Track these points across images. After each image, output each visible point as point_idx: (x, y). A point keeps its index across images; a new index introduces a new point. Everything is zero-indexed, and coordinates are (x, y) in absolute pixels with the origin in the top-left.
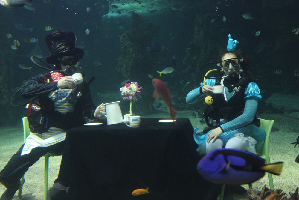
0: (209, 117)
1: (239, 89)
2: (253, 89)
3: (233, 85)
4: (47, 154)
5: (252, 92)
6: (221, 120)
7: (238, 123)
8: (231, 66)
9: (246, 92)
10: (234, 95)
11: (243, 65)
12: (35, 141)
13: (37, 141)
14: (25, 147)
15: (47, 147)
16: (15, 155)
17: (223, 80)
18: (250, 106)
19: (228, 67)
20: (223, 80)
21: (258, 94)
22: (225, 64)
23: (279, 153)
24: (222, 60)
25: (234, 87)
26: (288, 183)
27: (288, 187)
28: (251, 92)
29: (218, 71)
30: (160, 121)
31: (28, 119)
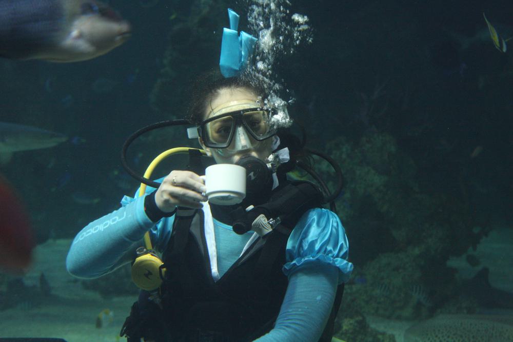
1: (271, 225)
2: (323, 232)
3: (251, 207)
5: (317, 247)
15: (92, 220)
21: (337, 256)
22: (218, 131)
24: (205, 119)
25: (255, 213)
28: (312, 244)
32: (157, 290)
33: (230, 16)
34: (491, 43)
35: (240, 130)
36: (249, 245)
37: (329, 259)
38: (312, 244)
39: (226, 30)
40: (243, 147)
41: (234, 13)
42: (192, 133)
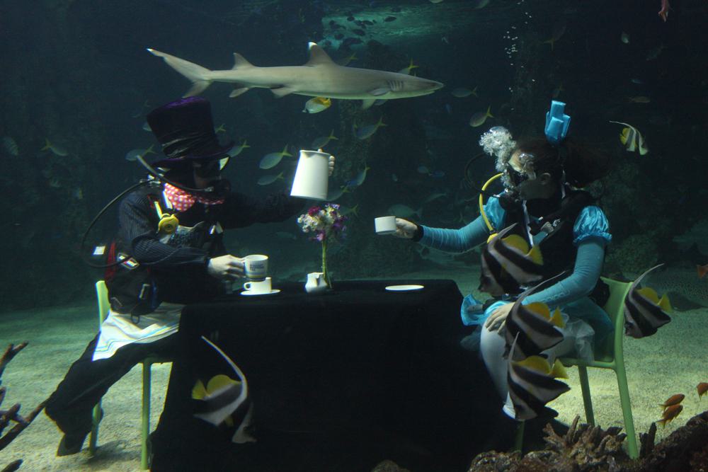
3: (541, 218)
4: (147, 360)
5: (590, 227)
7: (559, 295)
9: (576, 228)
12: (123, 332)
13: (128, 333)
14: (101, 344)
16: (76, 362)
18: (587, 258)
25: (543, 222)
28: (587, 227)
30: (388, 288)
31: (106, 282)
34: (506, 323)
37: (598, 234)
38: (587, 227)
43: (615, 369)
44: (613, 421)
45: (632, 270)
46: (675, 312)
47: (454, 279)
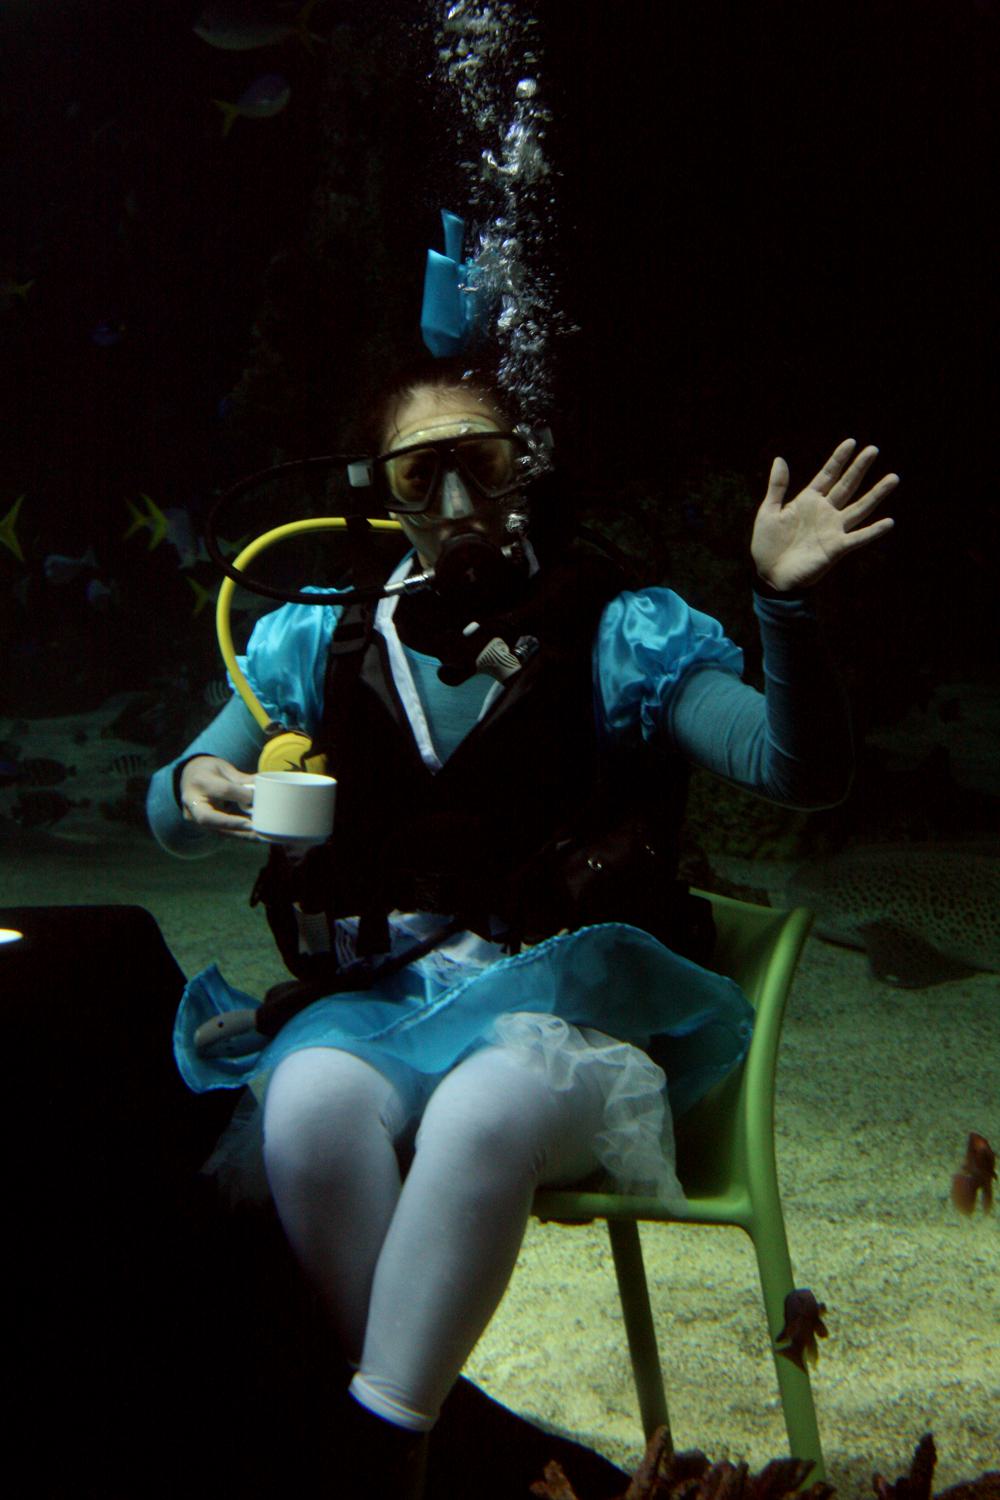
0: (297, 906)
1: (520, 657)
3: (473, 627)
6: (398, 920)
8: (454, 500)
10: (496, 715)
11: (537, 495)
17: (386, 610)
19: (435, 504)
20: (386, 610)
23: (946, 1157)
24: (385, 452)
26: (974, 1399)
27: (966, 1434)
29: (358, 526)
32: (989, 1148)
33: (446, 225)
35: (452, 478)
36: (496, 692)
39: (434, 255)
40: (456, 512)
41: (453, 218)
42: (357, 475)
43: (746, 1225)
44: (726, 1406)
45: (733, 845)
46: (892, 992)
47: (141, 904)
